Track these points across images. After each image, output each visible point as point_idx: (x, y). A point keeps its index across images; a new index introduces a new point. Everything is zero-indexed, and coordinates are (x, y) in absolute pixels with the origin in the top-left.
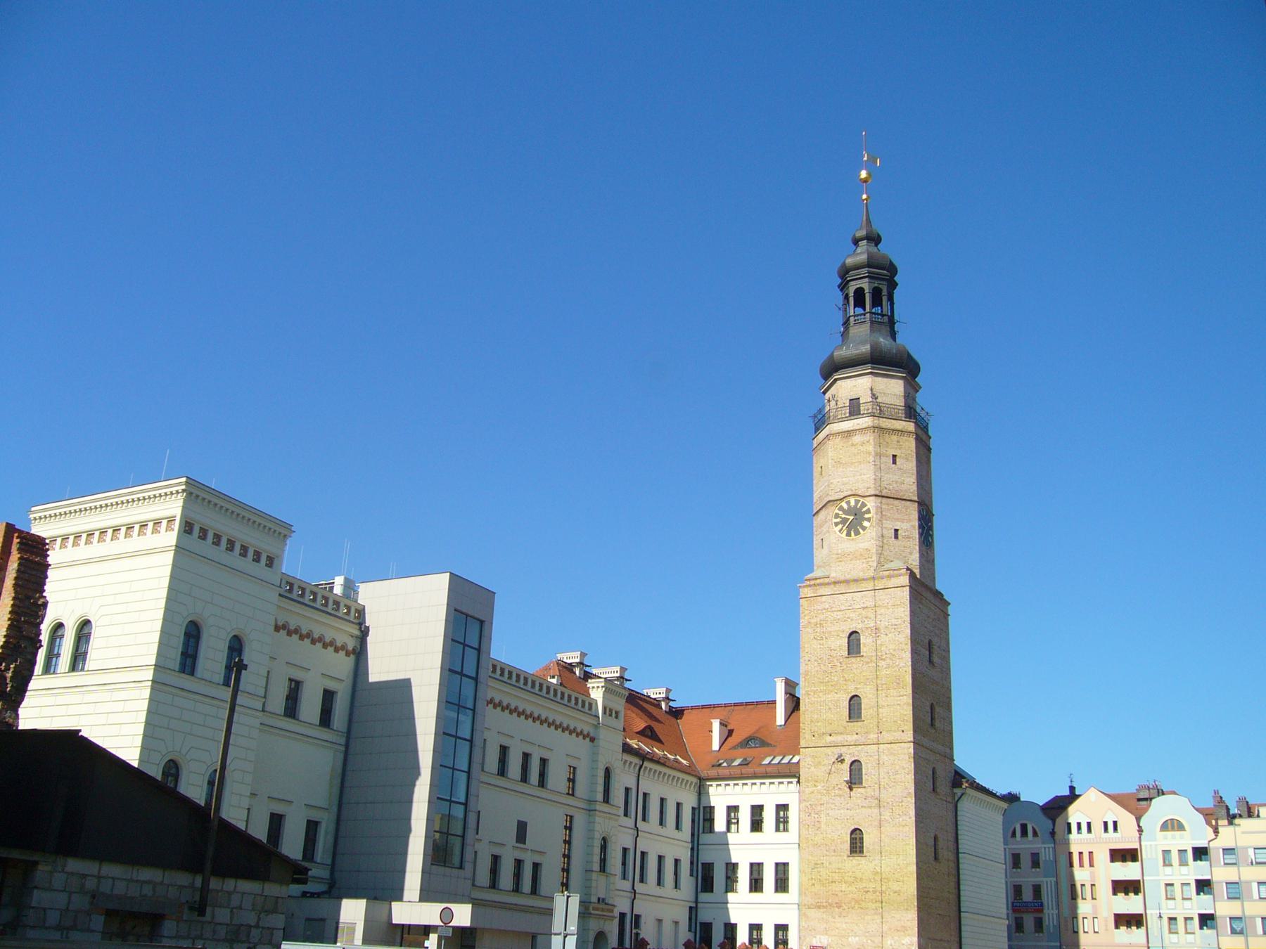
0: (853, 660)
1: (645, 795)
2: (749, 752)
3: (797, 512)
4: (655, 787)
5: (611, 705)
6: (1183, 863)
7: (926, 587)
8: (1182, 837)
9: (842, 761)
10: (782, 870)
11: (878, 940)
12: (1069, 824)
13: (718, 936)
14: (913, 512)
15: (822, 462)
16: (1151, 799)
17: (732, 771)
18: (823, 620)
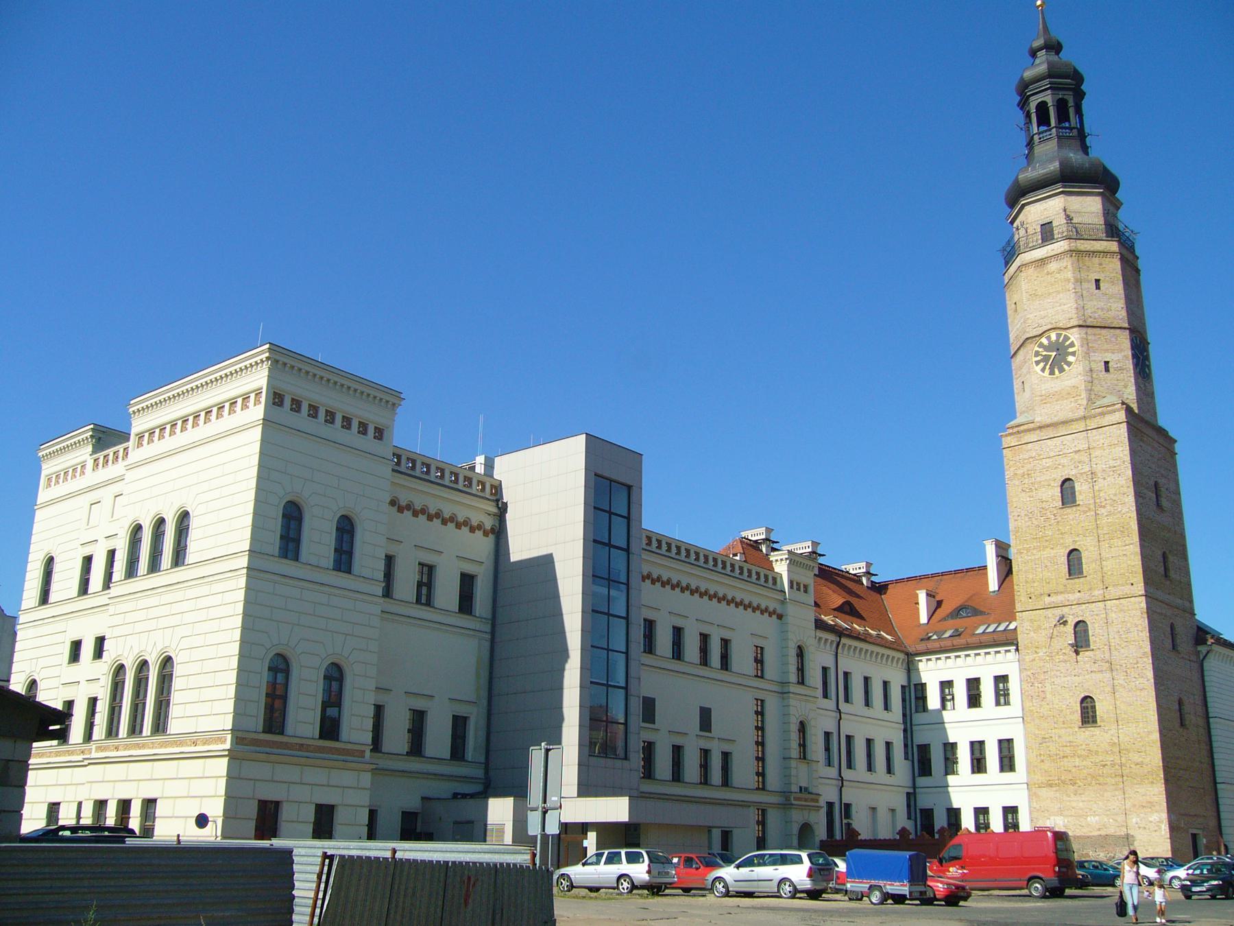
0: (1069, 510)
1: (846, 674)
2: (960, 623)
3: (991, 353)
4: (856, 664)
5: (796, 578)
7: (1147, 423)
10: (1006, 747)
11: (1121, 818)
13: (940, 821)
15: (1016, 298)
17: (943, 644)
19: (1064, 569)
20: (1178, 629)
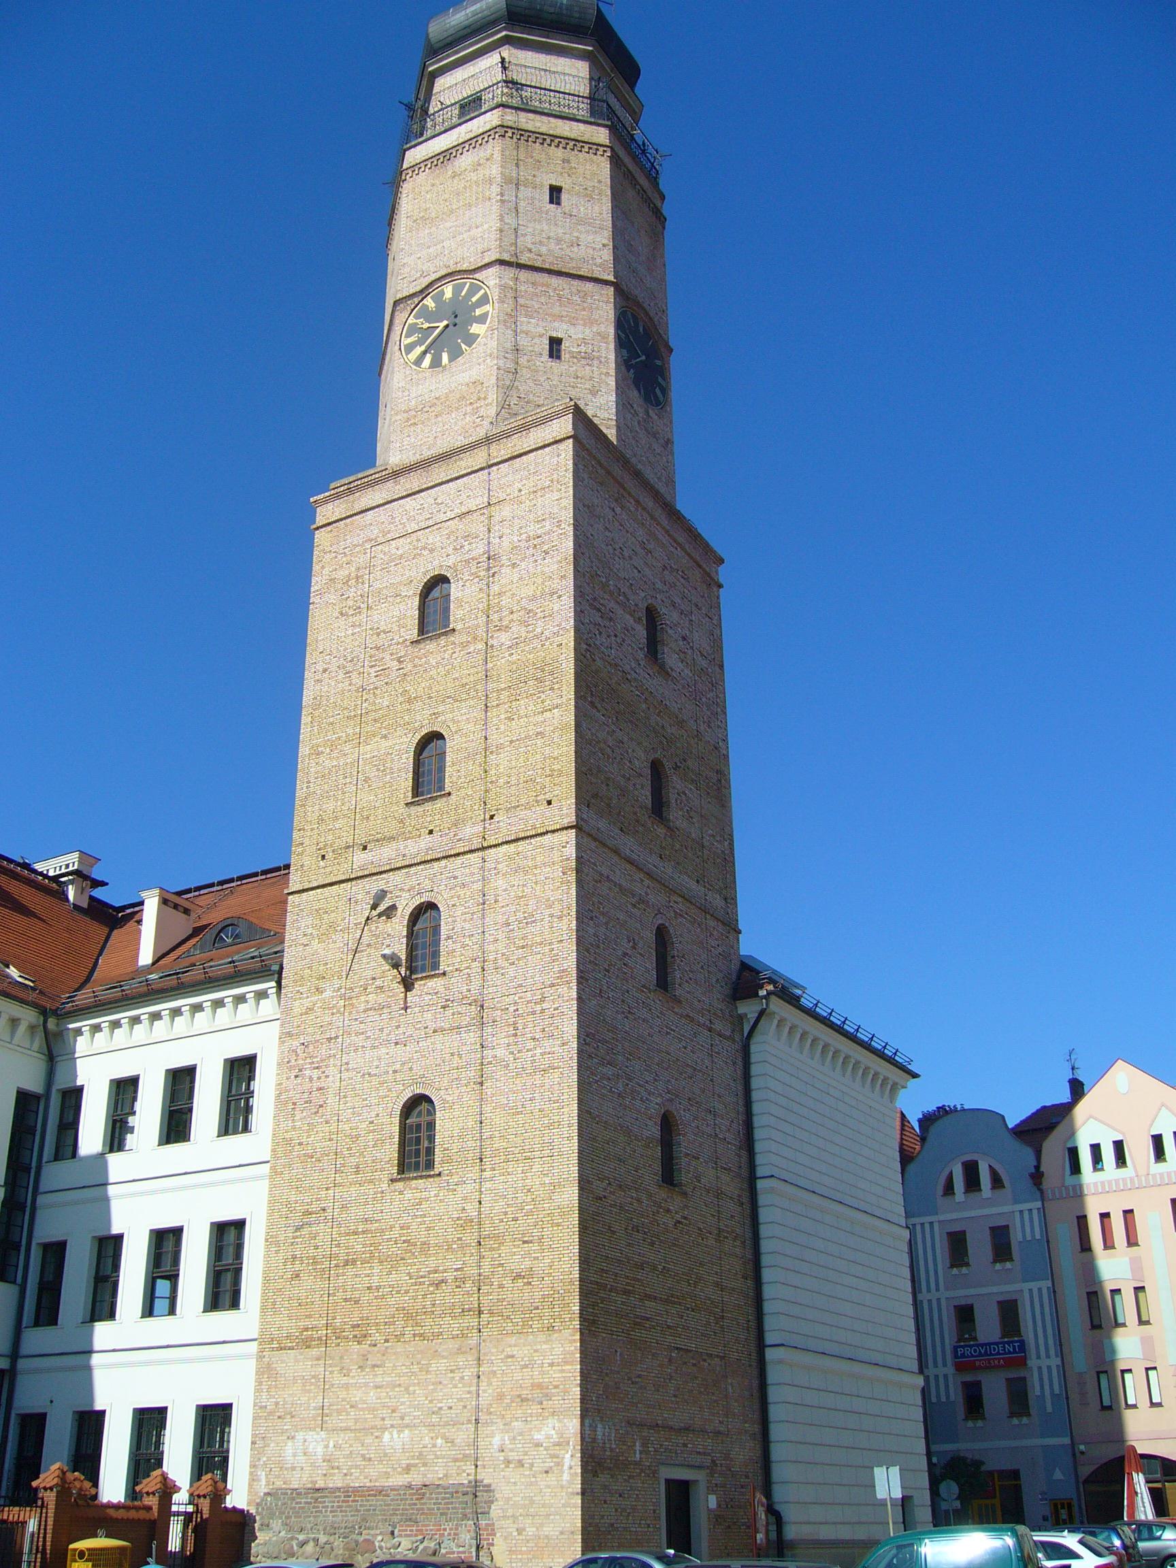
12: (1073, 1153)
19: (406, 782)
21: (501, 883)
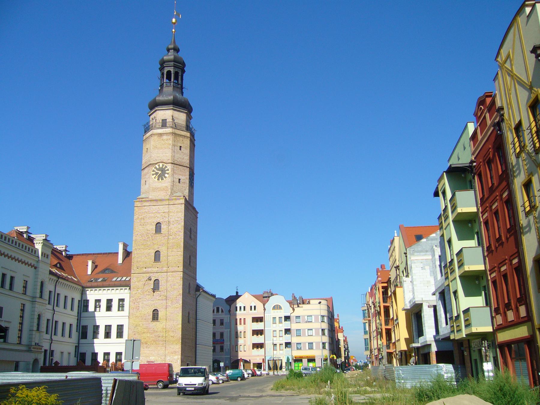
0: (158, 235)
2: (105, 276)
3: (134, 168)
6: (280, 322)
8: (280, 312)
9: (150, 280)
10: (120, 328)
12: (236, 307)
14: (187, 172)
15: (148, 146)
16: (269, 297)
17: (99, 284)
18: (144, 217)
20: (191, 285)
21: (170, 278)
